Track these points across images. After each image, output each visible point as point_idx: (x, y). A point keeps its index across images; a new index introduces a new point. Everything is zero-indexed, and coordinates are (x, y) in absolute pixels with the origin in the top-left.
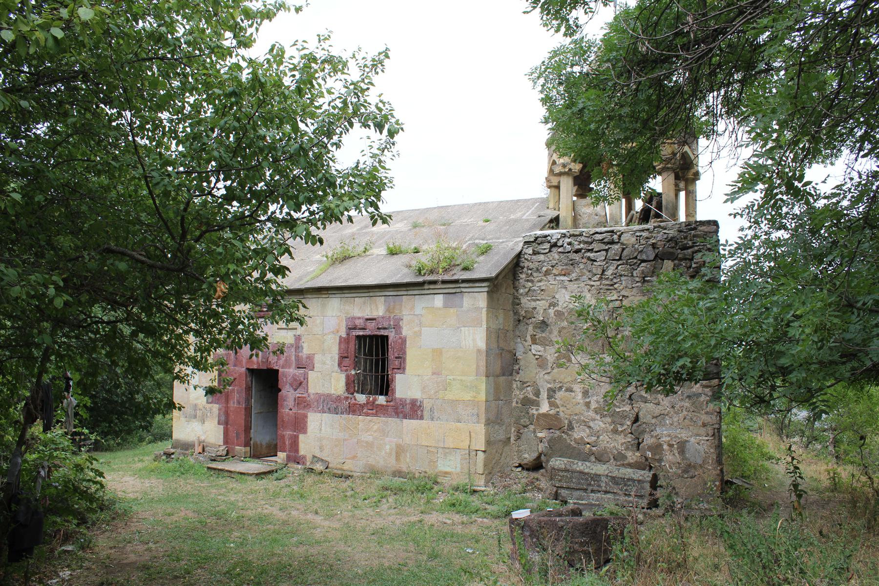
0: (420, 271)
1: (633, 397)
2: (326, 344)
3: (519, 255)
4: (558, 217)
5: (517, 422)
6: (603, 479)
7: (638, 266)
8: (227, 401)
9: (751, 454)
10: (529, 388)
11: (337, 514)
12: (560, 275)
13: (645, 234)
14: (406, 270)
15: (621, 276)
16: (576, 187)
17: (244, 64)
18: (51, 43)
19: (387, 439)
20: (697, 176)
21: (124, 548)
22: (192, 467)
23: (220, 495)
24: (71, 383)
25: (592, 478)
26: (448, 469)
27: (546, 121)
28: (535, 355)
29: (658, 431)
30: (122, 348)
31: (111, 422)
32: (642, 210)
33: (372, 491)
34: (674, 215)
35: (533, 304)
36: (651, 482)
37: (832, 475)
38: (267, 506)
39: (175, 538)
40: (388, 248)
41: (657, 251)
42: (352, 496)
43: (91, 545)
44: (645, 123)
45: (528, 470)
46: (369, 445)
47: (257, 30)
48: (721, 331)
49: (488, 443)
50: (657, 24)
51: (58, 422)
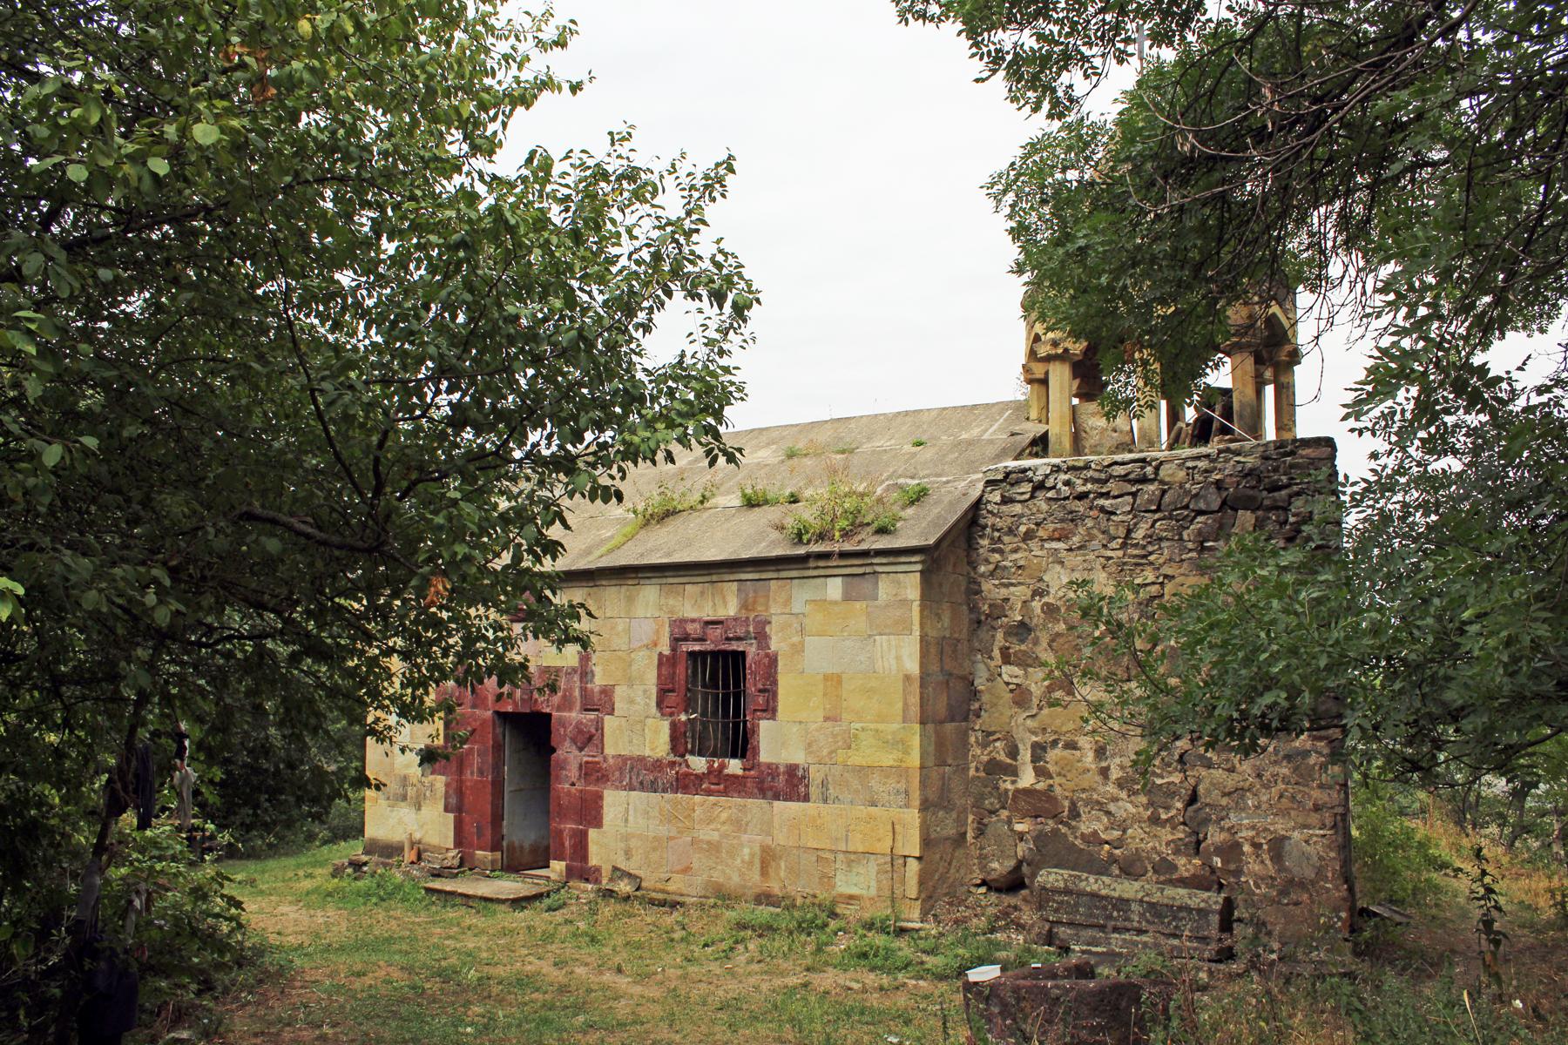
0: (799, 535)
1: (1186, 758)
2: (635, 667)
3: (978, 504)
4: (1046, 435)
5: (978, 805)
6: (1134, 907)
7: (1191, 522)
8: (460, 771)
9: (1407, 859)
10: (998, 744)
11: (655, 973)
12: (1051, 539)
13: (1202, 464)
14: (775, 535)
15: (1160, 539)
16: (1076, 383)
17: (481, 189)
18: (147, 184)
19: (745, 837)
20: (1295, 357)
21: (278, 1034)
22: (399, 887)
23: (449, 937)
24: (187, 743)
25: (1114, 906)
26: (854, 891)
27: (1019, 269)
28: (1008, 684)
29: (1233, 819)
30: (273, 682)
31: (256, 806)
32: (1196, 420)
33: (719, 930)
34: (1255, 428)
35: (1004, 592)
36: (1221, 913)
37: (1559, 898)
38: (531, 959)
39: (368, 1018)
40: (744, 495)
41: (1224, 494)
42: (682, 939)
43: (221, 1029)
44: (1198, 268)
45: (999, 890)
46: (713, 848)
47: (504, 125)
48: (1337, 642)
49: (926, 842)
50: (1212, 92)
51: (164, 809)
